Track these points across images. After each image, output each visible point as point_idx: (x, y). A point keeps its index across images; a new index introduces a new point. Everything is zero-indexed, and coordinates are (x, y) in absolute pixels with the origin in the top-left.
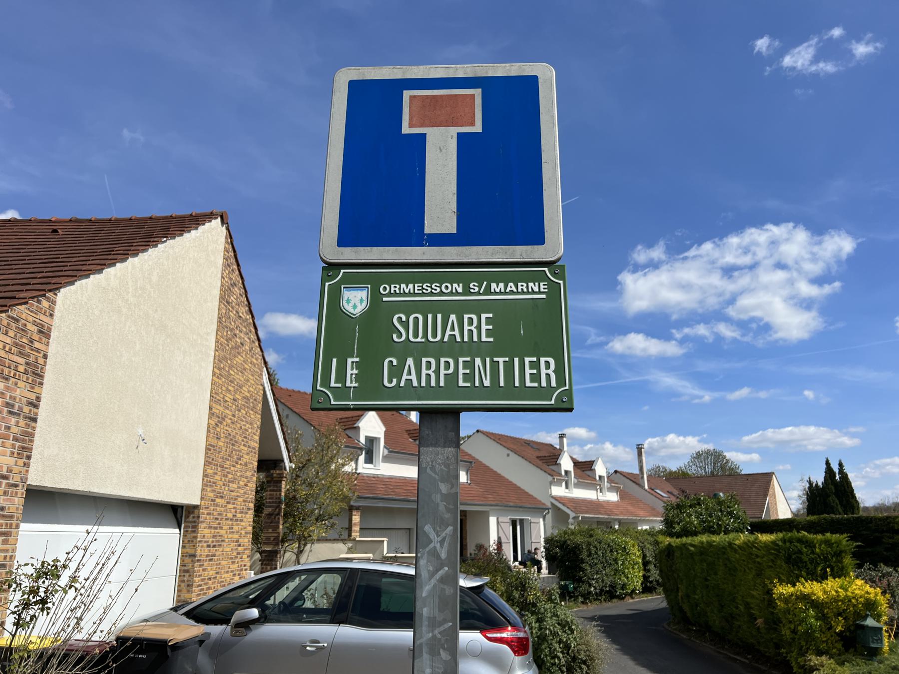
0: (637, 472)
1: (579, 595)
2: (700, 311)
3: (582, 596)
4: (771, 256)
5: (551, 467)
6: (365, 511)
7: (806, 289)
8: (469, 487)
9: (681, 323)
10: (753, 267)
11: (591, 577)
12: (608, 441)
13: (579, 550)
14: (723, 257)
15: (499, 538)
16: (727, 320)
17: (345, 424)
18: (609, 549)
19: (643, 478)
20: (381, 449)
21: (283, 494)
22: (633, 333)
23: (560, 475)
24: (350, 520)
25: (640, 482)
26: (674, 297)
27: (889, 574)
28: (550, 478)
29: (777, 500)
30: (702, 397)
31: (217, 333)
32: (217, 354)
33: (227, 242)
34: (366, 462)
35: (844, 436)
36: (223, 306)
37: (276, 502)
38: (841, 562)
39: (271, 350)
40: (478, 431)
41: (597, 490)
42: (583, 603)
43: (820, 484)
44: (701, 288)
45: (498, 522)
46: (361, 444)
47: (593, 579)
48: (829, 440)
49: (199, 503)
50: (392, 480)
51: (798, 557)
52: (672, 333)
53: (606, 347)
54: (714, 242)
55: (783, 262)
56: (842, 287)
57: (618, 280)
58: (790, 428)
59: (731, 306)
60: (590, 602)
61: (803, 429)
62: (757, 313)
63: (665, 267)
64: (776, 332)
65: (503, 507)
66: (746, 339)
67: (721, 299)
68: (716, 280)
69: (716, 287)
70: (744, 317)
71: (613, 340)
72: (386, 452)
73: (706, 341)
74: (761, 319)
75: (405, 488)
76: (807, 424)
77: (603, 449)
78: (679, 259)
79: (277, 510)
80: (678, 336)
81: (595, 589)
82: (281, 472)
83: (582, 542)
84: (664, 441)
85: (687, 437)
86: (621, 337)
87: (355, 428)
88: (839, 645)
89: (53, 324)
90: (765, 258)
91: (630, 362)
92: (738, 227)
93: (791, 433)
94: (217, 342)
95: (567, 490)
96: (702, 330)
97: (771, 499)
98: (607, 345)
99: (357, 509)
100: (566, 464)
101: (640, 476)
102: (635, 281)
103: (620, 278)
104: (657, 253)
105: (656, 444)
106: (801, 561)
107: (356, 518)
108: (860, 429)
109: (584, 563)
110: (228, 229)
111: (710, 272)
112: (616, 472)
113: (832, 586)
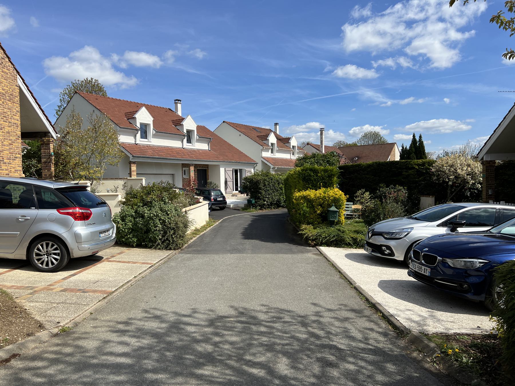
0: (319, 144)
1: (258, 206)
2: (390, 50)
4: (437, 13)
5: (263, 141)
6: (139, 165)
7: (454, 35)
8: (209, 152)
10: (425, 20)
11: (265, 196)
12: (331, 129)
13: (259, 183)
14: (407, 14)
15: (226, 179)
16: (405, 55)
17: (128, 116)
18: (277, 182)
19: (322, 147)
20: (151, 130)
21: (52, 151)
22: (350, 65)
23: (268, 145)
24: (130, 169)
25: (320, 149)
26: (374, 41)
27: (400, 190)
28: (261, 147)
29: (396, 158)
34: (142, 137)
35: (463, 124)
37: (48, 156)
38: (331, 180)
39: (133, 76)
40: (224, 122)
41: (290, 154)
42: (260, 209)
43: (408, 148)
45: (225, 171)
46: (137, 127)
47: (266, 198)
48: (454, 127)
50: (159, 148)
51: (309, 178)
52: (372, 63)
53: (332, 74)
54: (403, 4)
55: (443, 17)
56: (476, 34)
57: (342, 29)
58: (434, 120)
59: (408, 47)
60: (265, 209)
61: (441, 120)
63: (370, 21)
64: (433, 63)
65: (228, 162)
66: (414, 68)
67: (403, 42)
68: (401, 29)
69: (401, 35)
70: (415, 53)
71: (337, 69)
72: (154, 132)
73: (391, 69)
74: (425, 55)
75: (166, 152)
76: (444, 118)
77: (328, 134)
78: (378, 16)
79: (49, 160)
80: (375, 65)
82: (48, 139)
83: (260, 179)
84: (362, 129)
85: (375, 127)
86: (342, 67)
87: (133, 118)
90: (433, 14)
91: (347, 82)
93: (434, 123)
95: (272, 154)
96: (390, 62)
97: (392, 157)
98: (333, 72)
99: (134, 163)
100: (272, 139)
101: (321, 146)
102: (352, 30)
103: (342, 28)
104: (366, 12)
105: (357, 130)
106: (310, 180)
107: (134, 168)
108: (472, 120)
109: (261, 190)
111: (398, 24)
113: (320, 192)
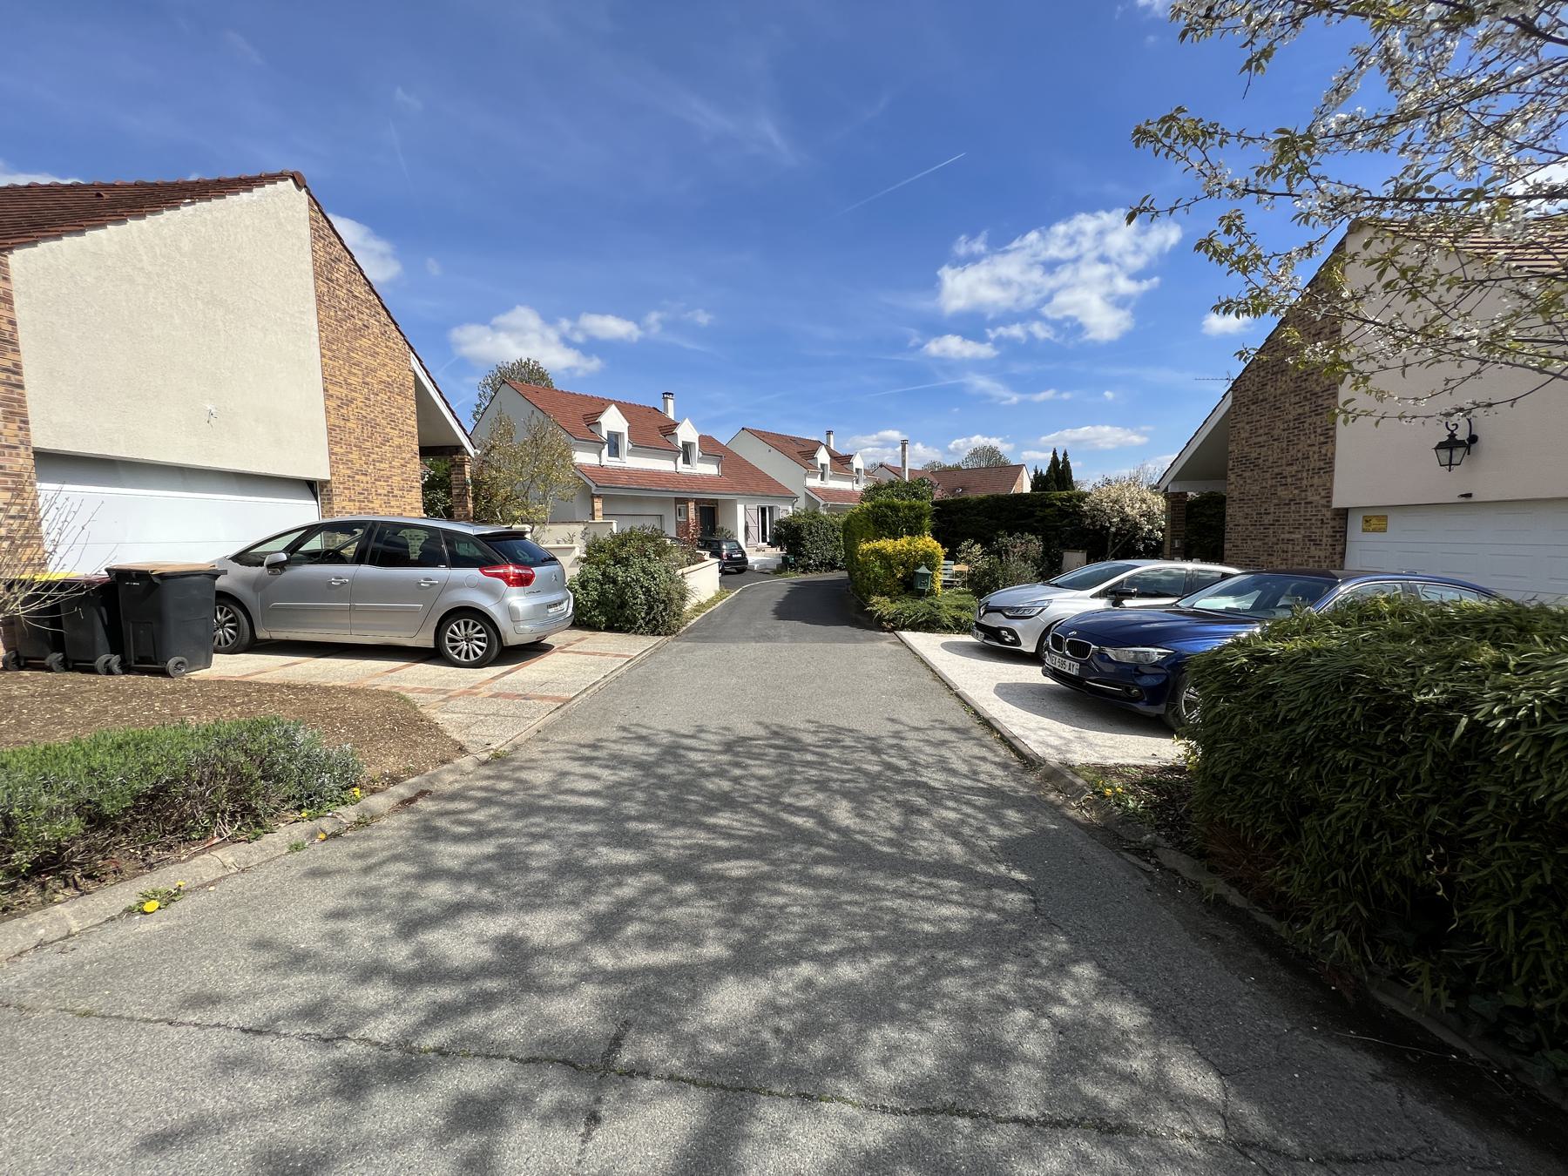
3: (802, 567)
4: (1097, 247)
6: (607, 499)
7: (1124, 286)
9: (994, 324)
10: (1076, 260)
14: (1046, 249)
15: (746, 523)
16: (1043, 319)
20: (625, 444)
21: (468, 477)
23: (816, 468)
26: (991, 295)
30: (1009, 399)
31: (318, 313)
32: (323, 334)
33: (312, 209)
36: (320, 282)
38: (920, 523)
43: (1045, 473)
44: (1020, 285)
49: (329, 478)
58: (1087, 428)
62: (1069, 312)
64: (1087, 333)
65: (750, 495)
66: (1057, 340)
67: (1039, 296)
68: (1036, 275)
70: (1058, 316)
76: (1103, 425)
80: (992, 336)
81: (814, 560)
84: (970, 441)
88: (900, 589)
89: (14, 288)
90: (1089, 250)
91: (948, 365)
92: (1066, 214)
94: (320, 322)
96: (1016, 331)
99: (599, 496)
100: (823, 457)
103: (939, 273)
104: (979, 246)
106: (887, 523)
107: (598, 505)
110: (308, 193)
112: (881, 466)
113: (902, 543)
